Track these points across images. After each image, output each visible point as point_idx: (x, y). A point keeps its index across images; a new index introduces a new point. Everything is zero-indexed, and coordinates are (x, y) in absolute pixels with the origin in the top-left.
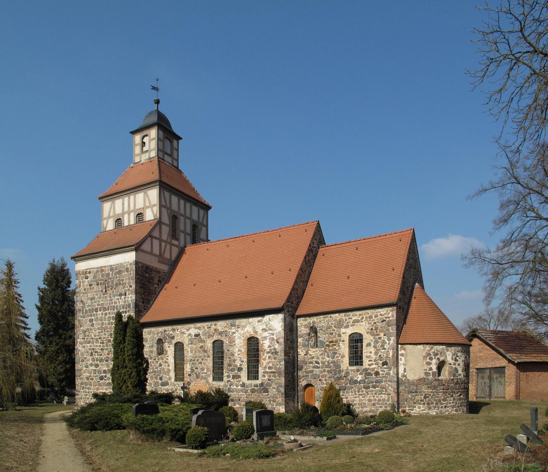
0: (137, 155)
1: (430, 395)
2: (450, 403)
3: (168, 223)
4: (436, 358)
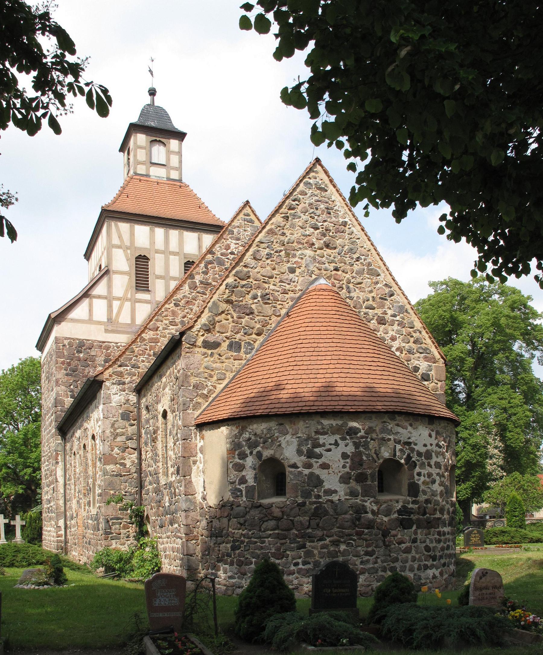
0: (168, 173)
1: (243, 542)
2: (296, 564)
3: (126, 268)
4: (254, 453)
